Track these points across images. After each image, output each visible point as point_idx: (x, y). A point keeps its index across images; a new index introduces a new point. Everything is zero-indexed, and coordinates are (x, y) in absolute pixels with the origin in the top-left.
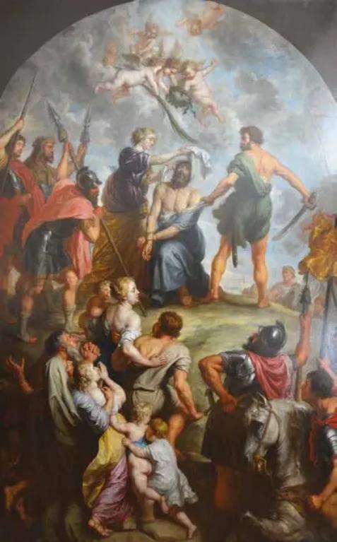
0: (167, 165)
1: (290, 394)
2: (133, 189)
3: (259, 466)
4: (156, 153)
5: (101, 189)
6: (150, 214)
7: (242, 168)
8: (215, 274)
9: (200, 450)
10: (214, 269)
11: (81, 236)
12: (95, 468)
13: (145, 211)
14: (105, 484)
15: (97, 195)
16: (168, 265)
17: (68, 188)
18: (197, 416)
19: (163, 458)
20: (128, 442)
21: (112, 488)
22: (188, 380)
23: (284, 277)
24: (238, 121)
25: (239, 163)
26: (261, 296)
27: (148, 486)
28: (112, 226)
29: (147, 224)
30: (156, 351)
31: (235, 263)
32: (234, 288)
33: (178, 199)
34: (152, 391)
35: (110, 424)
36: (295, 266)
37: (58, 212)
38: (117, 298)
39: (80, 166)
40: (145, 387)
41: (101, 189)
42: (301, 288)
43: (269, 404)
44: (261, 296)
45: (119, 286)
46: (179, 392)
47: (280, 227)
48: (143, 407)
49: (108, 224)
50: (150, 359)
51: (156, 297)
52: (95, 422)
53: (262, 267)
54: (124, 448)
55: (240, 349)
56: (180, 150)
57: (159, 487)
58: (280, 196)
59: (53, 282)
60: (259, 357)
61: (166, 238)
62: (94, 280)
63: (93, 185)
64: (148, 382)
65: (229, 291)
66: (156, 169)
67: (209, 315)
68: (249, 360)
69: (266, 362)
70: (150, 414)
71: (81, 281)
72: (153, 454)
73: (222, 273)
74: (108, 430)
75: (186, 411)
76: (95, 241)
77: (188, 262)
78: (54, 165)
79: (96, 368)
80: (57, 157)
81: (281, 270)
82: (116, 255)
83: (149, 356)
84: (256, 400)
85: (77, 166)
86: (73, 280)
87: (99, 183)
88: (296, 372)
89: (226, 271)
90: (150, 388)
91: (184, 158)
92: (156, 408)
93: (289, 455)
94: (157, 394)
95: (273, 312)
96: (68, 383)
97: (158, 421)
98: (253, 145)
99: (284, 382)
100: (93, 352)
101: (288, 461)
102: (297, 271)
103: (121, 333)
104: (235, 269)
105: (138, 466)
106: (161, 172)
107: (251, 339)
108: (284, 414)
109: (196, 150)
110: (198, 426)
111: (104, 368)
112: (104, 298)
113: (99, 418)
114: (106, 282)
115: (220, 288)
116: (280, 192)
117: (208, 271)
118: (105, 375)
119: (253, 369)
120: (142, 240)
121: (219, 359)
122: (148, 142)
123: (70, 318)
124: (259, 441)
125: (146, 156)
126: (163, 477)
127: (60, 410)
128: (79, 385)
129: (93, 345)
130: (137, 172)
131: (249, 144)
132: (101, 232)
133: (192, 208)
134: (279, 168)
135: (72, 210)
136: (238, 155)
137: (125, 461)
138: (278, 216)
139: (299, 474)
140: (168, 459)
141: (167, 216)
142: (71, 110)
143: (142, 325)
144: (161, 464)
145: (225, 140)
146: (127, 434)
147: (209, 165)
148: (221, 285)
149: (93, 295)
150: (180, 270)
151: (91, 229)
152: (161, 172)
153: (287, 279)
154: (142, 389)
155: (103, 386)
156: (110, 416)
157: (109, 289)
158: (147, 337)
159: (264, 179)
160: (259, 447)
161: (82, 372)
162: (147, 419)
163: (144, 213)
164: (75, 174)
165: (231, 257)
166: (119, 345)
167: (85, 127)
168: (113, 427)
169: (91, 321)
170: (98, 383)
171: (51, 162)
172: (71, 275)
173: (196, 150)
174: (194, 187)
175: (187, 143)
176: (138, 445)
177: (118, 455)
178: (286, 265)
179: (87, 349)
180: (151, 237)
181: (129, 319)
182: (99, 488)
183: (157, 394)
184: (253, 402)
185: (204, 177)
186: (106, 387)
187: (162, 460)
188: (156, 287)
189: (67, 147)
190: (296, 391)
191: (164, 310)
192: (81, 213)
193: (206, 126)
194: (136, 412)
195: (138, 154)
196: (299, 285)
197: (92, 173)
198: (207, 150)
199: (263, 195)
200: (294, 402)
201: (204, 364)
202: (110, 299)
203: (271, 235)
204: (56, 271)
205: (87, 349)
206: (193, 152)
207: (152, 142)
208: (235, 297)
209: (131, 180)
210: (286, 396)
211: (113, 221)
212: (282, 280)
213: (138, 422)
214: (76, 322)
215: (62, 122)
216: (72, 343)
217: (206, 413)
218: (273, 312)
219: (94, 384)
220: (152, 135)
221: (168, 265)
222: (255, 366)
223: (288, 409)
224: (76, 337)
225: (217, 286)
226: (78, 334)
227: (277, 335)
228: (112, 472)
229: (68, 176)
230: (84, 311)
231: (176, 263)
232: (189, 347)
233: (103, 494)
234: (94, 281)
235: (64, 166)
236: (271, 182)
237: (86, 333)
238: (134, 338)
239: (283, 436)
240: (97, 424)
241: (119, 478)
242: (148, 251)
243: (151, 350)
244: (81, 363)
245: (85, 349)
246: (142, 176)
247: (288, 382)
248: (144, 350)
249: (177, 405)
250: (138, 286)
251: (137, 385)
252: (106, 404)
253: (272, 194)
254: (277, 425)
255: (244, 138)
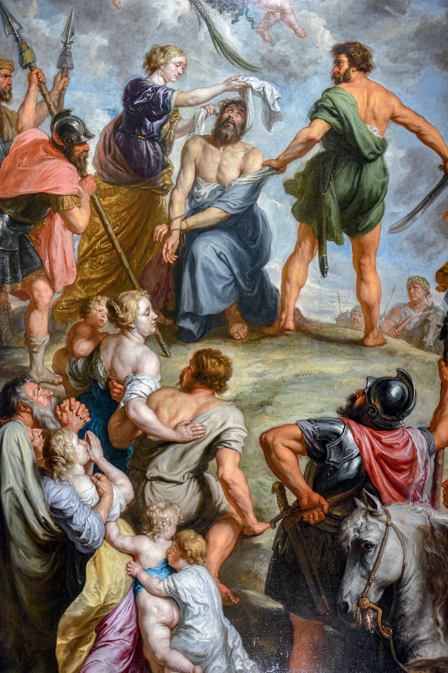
0: (204, 107)
1: (422, 494)
2: (145, 145)
3: (369, 619)
4: (187, 88)
5: (93, 145)
6: (176, 187)
7: (334, 111)
8: (288, 286)
9: (263, 587)
10: (286, 278)
11: (58, 222)
12: (79, 613)
13: (167, 182)
14: (97, 640)
15: (86, 157)
16: (206, 270)
17: (36, 143)
18: (258, 527)
19: (197, 597)
20: (136, 569)
21: (108, 647)
22: (242, 466)
23: (411, 296)
24: (328, 35)
25: (329, 104)
26: (370, 328)
27: (172, 648)
28: (110, 206)
29: (171, 202)
30: (185, 415)
31: (324, 270)
32: (322, 312)
33: (224, 163)
34: (181, 483)
35: (106, 538)
36: (431, 277)
37: (18, 184)
38: (118, 326)
39: (57, 108)
40: (167, 477)
41: (93, 145)
42: (440, 314)
43: (387, 513)
44: (370, 328)
45: (121, 305)
46: (226, 486)
47: (403, 211)
48: (162, 510)
49: (105, 203)
50: (175, 428)
51: (187, 324)
52: (79, 534)
53: (370, 276)
54: (131, 580)
55: (334, 415)
56: (228, 82)
57: (191, 650)
58: (402, 160)
59: (10, 296)
60: (366, 430)
61: (201, 226)
62: (80, 294)
63: (79, 139)
64: (171, 468)
65: (314, 317)
66: (186, 114)
67: (278, 356)
68: (350, 435)
69: (379, 439)
70: (175, 522)
71: (57, 296)
72: (180, 592)
73: (300, 286)
74: (102, 548)
75: (239, 519)
76: (82, 231)
77: (241, 265)
78: (13, 107)
79: (84, 442)
80: (18, 93)
81: (404, 283)
82: (118, 254)
83: (174, 423)
84: (361, 504)
85: (52, 107)
86: (44, 294)
87: (90, 136)
88: (434, 456)
89: (308, 283)
90: (177, 478)
91: (235, 96)
92: (187, 511)
93: (423, 601)
94: (188, 486)
95: (391, 353)
96: (35, 466)
97: (189, 534)
98: (354, 74)
99: (412, 475)
100: (77, 415)
101: (420, 614)
102: (433, 286)
103: (124, 383)
104: (323, 280)
105: (155, 610)
106: (194, 118)
107: (353, 399)
108: (413, 530)
109: (255, 82)
110: (258, 546)
111: (95, 441)
112: (94, 327)
113: (87, 527)
114: (99, 298)
115: (297, 311)
116: (402, 153)
117: (276, 282)
118: (97, 453)
119: (356, 451)
120: (162, 229)
121: (297, 432)
122: (172, 69)
123: (39, 357)
124: (369, 576)
125: (170, 93)
126: (198, 632)
127: (20, 512)
128: (53, 470)
129: (78, 403)
130: (153, 119)
131: (347, 71)
132: (92, 215)
133: (248, 178)
134: (399, 111)
135: (44, 179)
136: (328, 90)
137: (132, 601)
138: (400, 192)
139: (442, 637)
140: (206, 600)
141: (205, 190)
142: (41, 16)
143: (161, 371)
144: (195, 609)
145: (304, 65)
146: (135, 556)
147: (277, 108)
148: (298, 305)
149: (80, 320)
150: (227, 279)
151: (76, 211)
152: (194, 118)
153: (415, 299)
154: (161, 479)
155: (94, 472)
156: (106, 524)
157: (106, 310)
158: (171, 392)
159: (375, 131)
160: (369, 584)
161: (58, 449)
162: (170, 531)
163: (165, 185)
164: (48, 121)
165: (316, 259)
166: (122, 404)
167: (65, 44)
168: (112, 543)
169: (75, 362)
170: (86, 467)
171: (7, 101)
172: (41, 285)
173: (255, 82)
174: (252, 142)
175: (243, 72)
176: (155, 575)
177: (119, 592)
178: (413, 274)
179: (67, 409)
180: (176, 224)
181: (138, 361)
182: (86, 648)
183: (188, 486)
184: (355, 506)
185: (269, 127)
186: (99, 475)
187: (197, 602)
188: (187, 306)
189: (35, 77)
190: (434, 488)
191: (199, 347)
192: (60, 185)
193: (272, 43)
194: (150, 519)
195: (156, 89)
196: (437, 309)
197: (77, 119)
198: (273, 82)
199: (372, 157)
200: (430, 510)
201: (270, 438)
202: (107, 327)
203: (386, 224)
204: (15, 279)
205: (67, 409)
206: (251, 87)
207: (180, 69)
208: (322, 326)
209: (144, 133)
210: (415, 499)
211: (113, 199)
212: (407, 300)
213: (154, 535)
214: (49, 363)
215: (24, 35)
216: (41, 399)
217: (273, 523)
218: (391, 353)
219: (79, 469)
220: (179, 59)
221: (206, 270)
222: (360, 446)
223: (418, 521)
224: (49, 389)
225: (291, 309)
226: (53, 383)
227: (398, 394)
228: (108, 622)
229: (37, 124)
230: (63, 345)
231: (221, 269)
232: (242, 410)
233: (91, 659)
234: (79, 296)
235: (31, 106)
236: (387, 137)
237: (65, 383)
238: (148, 392)
239: (412, 568)
240: (83, 536)
241: (121, 631)
242: (173, 246)
243: (177, 414)
244: (56, 432)
245: (63, 410)
246: (162, 126)
247: (420, 475)
248: (165, 413)
249: (222, 508)
250: (155, 305)
251: (151, 473)
252: (99, 502)
253: (388, 154)
254: (400, 548)
255: (338, 63)
